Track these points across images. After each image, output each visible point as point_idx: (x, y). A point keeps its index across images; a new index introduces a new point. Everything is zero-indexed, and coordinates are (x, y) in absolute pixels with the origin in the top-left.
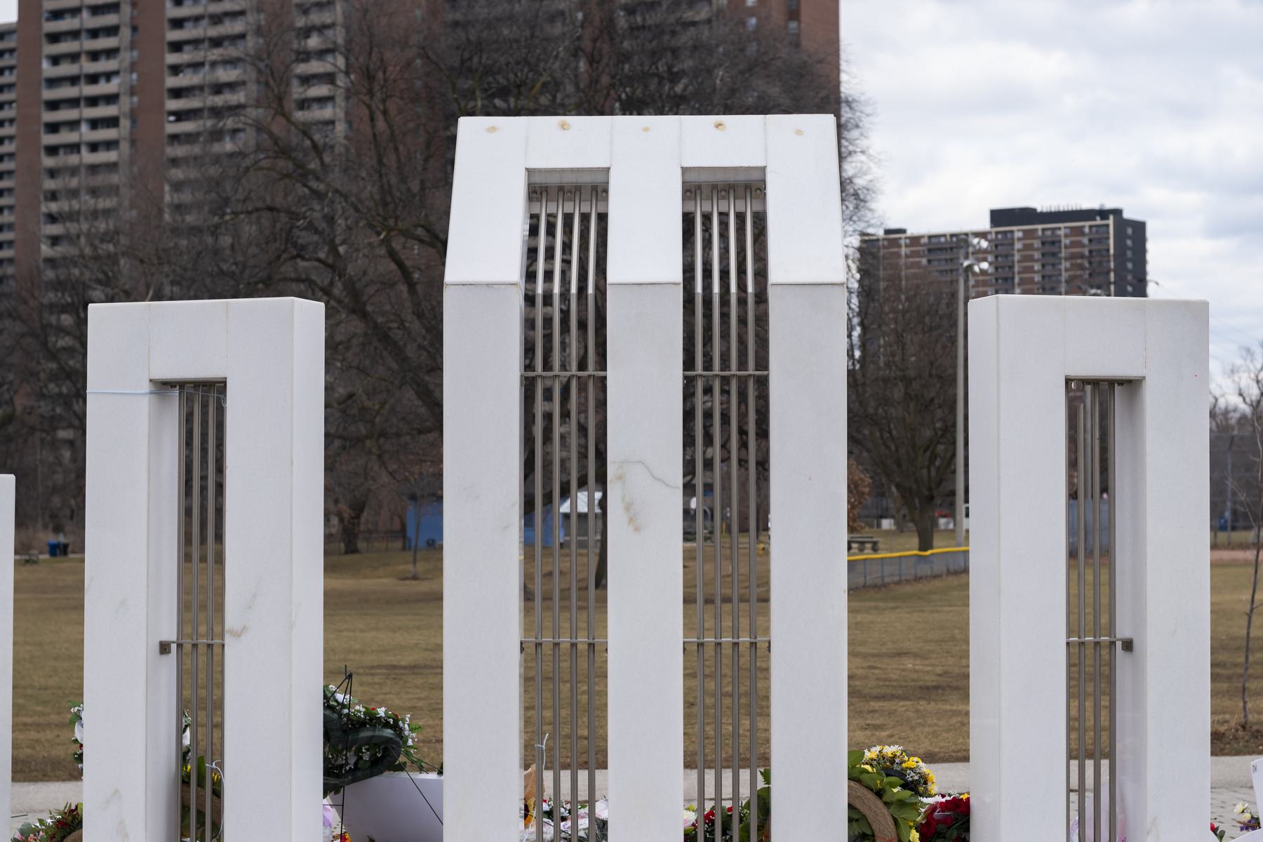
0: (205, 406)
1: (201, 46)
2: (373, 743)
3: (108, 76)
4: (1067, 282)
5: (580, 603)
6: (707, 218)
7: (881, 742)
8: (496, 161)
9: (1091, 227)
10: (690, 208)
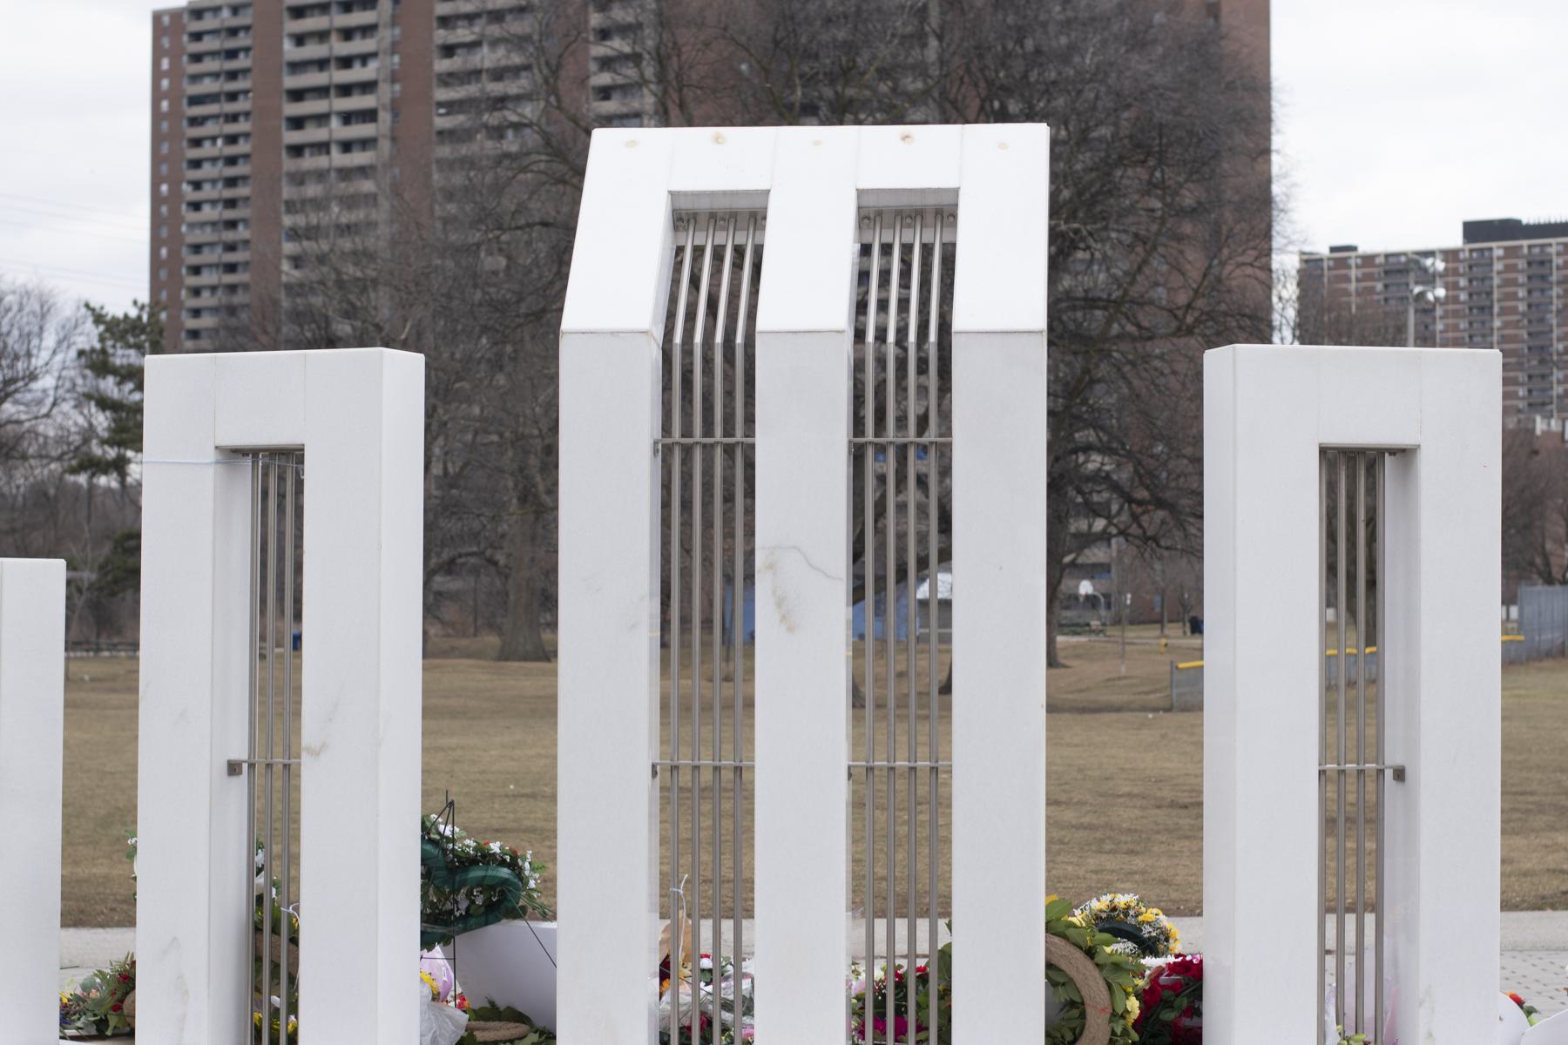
0: (282, 479)
2: (488, 886)
3: (364, 58)
4: (1558, 311)
5: (920, 712)
7: (1109, 888)
8: (634, 180)
10: (866, 240)
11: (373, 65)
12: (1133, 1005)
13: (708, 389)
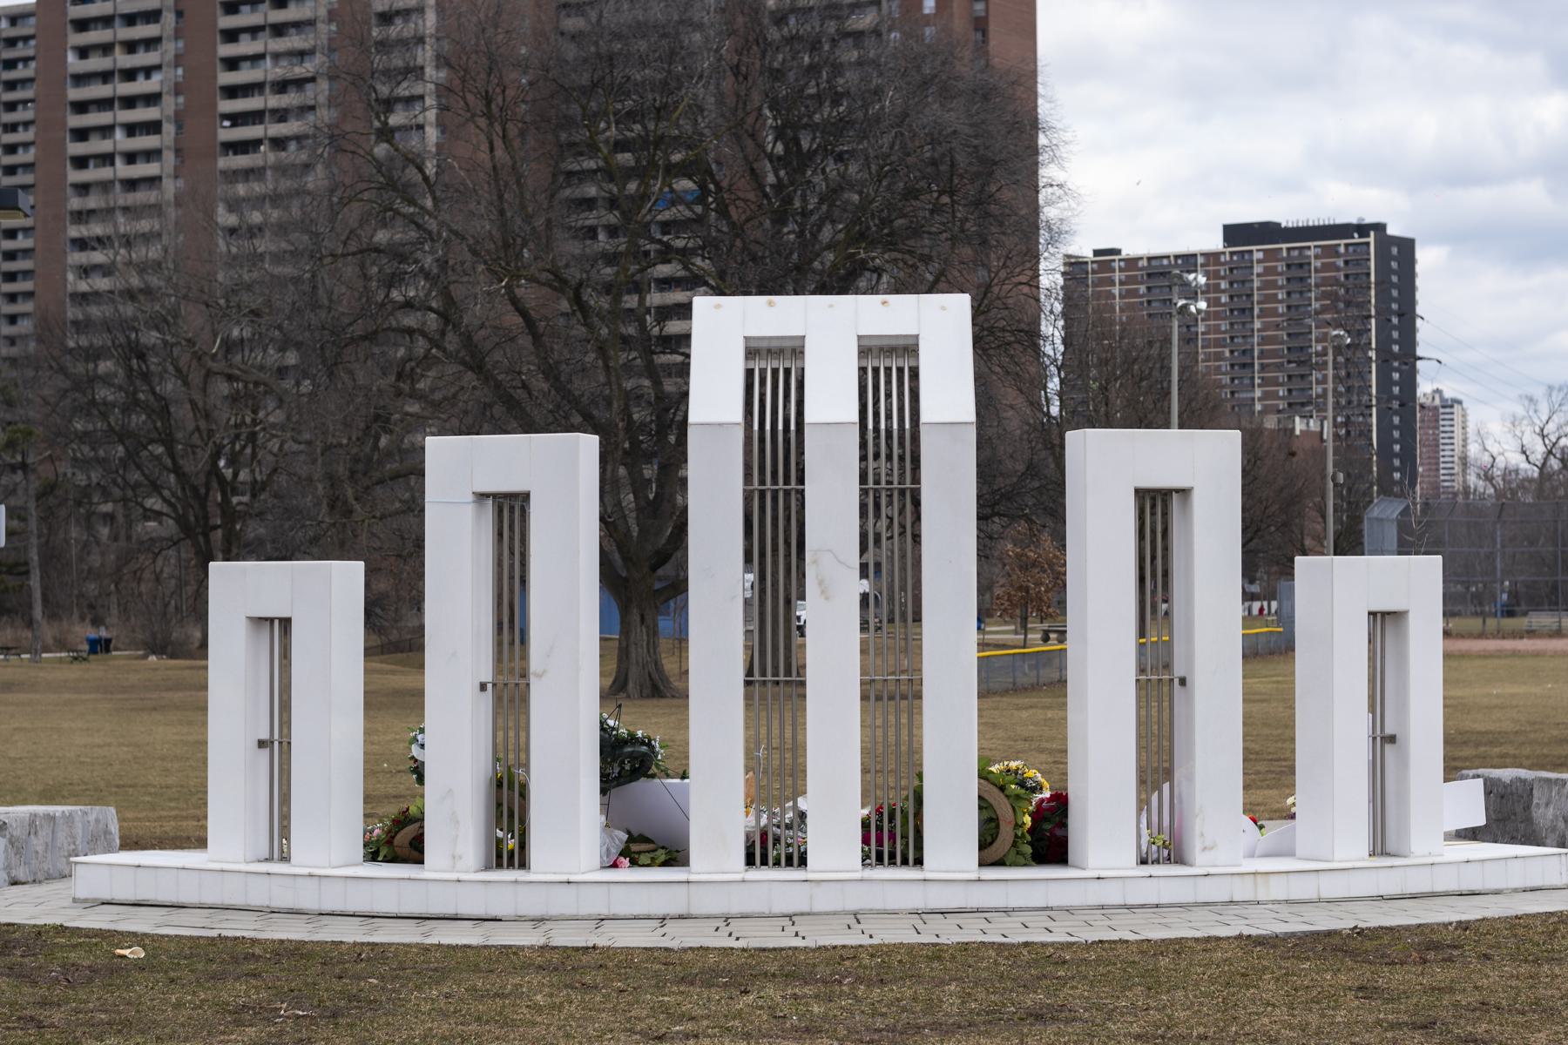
1: (261, 34)
3: (148, 71)
6: (876, 371)
8: (722, 332)
9: (1347, 245)
11: (157, 78)
12: (1028, 820)
13: (776, 456)
